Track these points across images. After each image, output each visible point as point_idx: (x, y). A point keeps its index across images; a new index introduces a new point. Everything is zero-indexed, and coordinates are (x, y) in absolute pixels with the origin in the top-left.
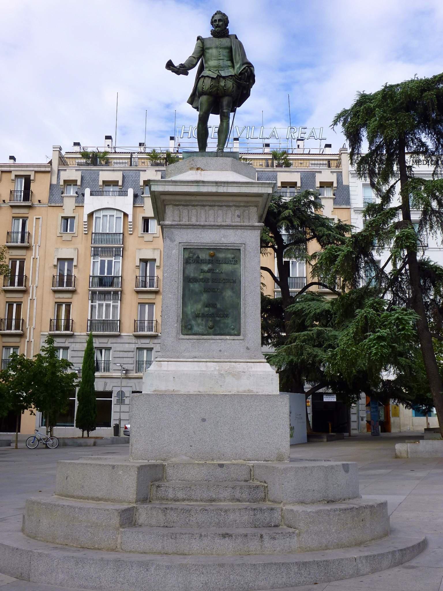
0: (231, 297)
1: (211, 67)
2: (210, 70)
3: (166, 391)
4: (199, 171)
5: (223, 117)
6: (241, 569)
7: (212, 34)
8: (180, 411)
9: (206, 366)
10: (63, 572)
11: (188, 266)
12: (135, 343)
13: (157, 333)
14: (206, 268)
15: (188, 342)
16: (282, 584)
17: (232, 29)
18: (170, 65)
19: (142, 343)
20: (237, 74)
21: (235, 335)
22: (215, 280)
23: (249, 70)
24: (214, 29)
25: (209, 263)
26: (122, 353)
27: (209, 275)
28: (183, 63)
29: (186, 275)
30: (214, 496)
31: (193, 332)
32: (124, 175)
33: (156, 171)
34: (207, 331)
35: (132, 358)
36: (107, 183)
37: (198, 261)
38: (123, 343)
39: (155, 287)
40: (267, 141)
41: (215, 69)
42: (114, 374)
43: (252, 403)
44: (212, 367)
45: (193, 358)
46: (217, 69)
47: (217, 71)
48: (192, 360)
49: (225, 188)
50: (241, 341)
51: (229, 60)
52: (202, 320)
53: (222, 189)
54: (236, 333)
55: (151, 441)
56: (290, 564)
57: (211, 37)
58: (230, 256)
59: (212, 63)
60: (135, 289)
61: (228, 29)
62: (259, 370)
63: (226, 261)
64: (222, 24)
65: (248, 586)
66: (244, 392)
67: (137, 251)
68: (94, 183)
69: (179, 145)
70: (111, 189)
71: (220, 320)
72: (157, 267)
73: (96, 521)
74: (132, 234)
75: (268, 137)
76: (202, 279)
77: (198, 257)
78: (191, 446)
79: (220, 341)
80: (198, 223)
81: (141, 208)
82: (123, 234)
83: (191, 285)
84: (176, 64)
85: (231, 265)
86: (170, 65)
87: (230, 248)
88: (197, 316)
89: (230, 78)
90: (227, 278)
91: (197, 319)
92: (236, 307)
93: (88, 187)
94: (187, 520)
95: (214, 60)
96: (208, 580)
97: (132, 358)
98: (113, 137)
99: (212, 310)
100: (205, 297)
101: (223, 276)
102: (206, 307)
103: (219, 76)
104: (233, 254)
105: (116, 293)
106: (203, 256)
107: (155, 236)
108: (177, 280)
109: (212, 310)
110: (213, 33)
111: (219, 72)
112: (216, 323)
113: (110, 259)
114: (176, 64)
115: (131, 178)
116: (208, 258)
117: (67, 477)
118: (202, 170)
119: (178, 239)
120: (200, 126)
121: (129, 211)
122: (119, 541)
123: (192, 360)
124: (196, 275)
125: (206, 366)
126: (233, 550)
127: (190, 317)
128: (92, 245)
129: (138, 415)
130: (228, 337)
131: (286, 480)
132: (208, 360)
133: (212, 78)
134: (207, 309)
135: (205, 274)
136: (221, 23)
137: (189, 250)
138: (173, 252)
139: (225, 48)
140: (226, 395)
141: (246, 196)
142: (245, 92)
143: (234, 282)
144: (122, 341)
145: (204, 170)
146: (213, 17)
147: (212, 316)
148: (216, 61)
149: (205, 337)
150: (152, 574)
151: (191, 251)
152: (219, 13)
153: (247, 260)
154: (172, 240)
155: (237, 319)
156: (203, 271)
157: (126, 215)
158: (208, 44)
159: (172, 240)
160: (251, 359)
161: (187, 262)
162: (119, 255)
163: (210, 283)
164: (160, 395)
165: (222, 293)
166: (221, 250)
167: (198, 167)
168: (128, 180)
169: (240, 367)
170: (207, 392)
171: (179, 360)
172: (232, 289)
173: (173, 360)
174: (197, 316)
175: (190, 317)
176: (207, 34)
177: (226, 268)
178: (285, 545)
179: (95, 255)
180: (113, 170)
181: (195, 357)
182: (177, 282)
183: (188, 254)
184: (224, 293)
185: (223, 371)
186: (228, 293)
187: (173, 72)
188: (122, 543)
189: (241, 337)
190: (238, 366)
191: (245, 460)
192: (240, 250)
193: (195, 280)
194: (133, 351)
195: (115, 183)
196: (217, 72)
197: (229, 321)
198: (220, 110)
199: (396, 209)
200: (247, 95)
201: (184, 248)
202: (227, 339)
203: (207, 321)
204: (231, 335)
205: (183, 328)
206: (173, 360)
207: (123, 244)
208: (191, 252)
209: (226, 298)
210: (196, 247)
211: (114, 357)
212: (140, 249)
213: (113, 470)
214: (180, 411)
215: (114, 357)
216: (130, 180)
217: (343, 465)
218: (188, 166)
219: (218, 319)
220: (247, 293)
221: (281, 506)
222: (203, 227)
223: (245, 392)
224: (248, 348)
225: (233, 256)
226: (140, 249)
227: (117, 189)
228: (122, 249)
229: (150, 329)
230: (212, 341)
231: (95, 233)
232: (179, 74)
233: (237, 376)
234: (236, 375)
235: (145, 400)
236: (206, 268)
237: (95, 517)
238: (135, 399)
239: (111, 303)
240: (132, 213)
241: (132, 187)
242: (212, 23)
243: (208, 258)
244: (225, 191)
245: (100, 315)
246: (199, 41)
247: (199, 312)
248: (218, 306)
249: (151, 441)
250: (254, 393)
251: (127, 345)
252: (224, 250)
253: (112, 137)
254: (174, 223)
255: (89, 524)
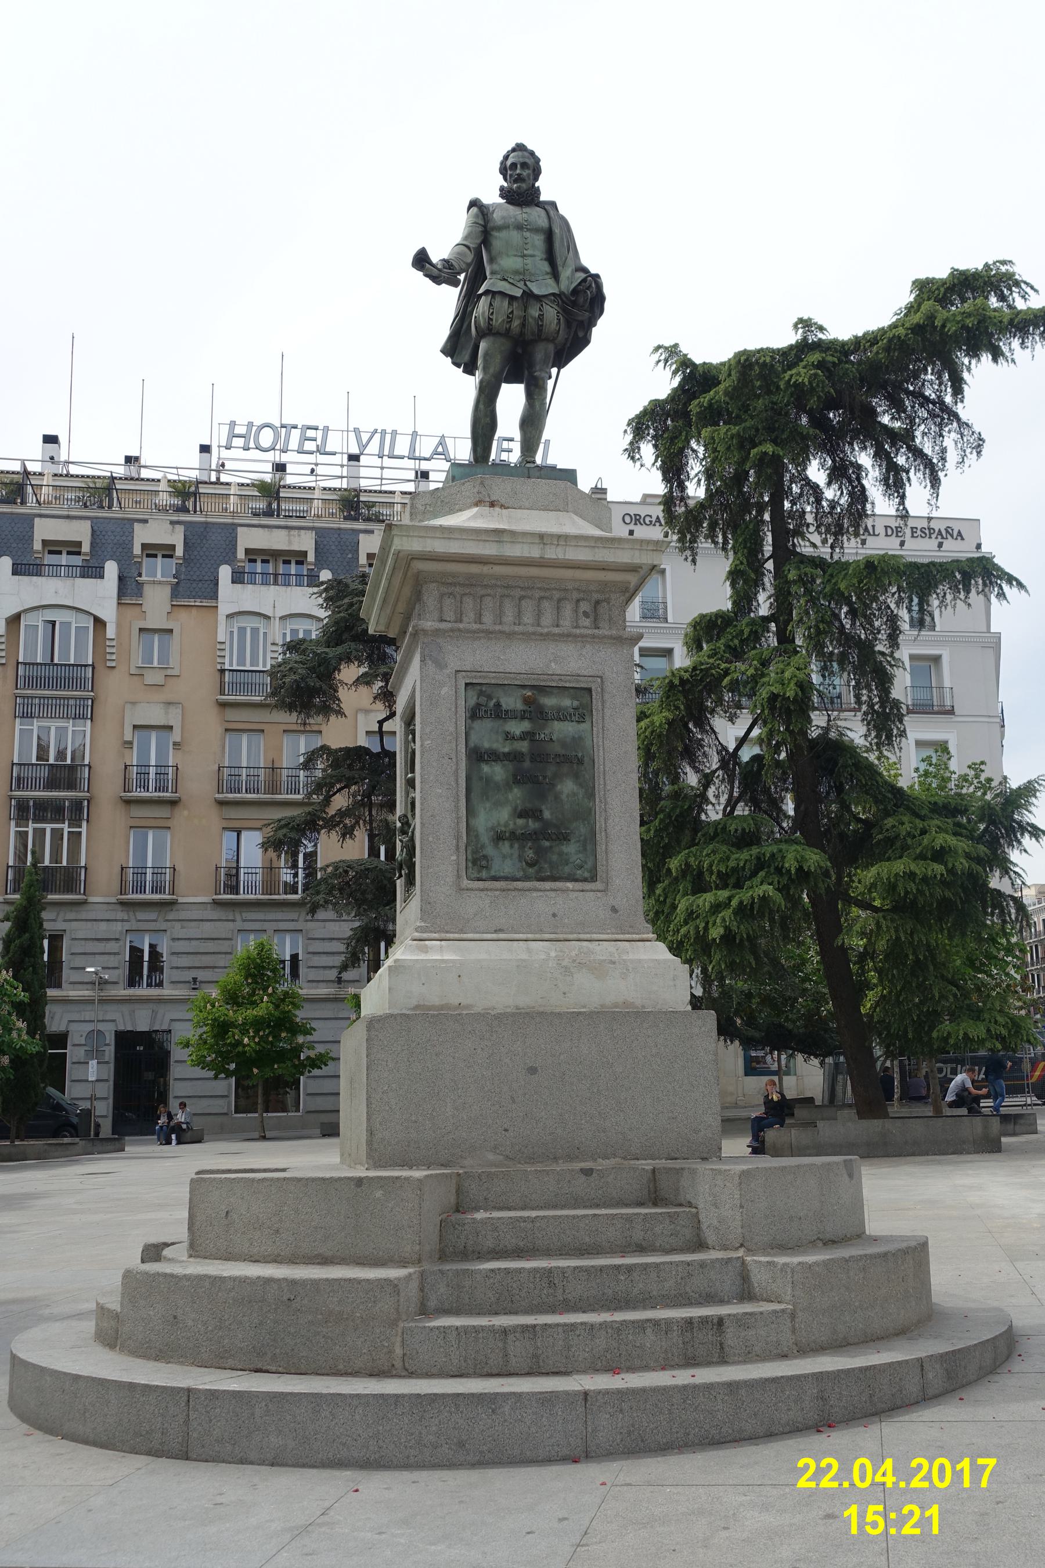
0: (574, 794)
1: (506, 271)
2: (505, 280)
3: (442, 1007)
4: (497, 509)
5: (532, 388)
6: (704, 1395)
7: (502, 196)
8: (479, 1051)
9: (528, 948)
10: (280, 1431)
11: (477, 724)
12: (123, 921)
13: (174, 897)
14: (517, 728)
15: (482, 894)
16: (788, 1424)
17: (547, 188)
18: (421, 260)
19: (139, 921)
20: (566, 292)
21: (585, 880)
22: (539, 757)
23: (593, 285)
24: (505, 185)
25: (523, 718)
26: (91, 943)
27: (524, 746)
28: (446, 257)
29: (472, 745)
30: (587, 1239)
31: (493, 873)
32: (95, 528)
33: (172, 523)
34: (524, 870)
35: (115, 954)
36: (53, 547)
37: (499, 713)
38: (95, 920)
39: (170, 790)
40: (425, 466)
41: (517, 278)
42: (72, 993)
43: (637, 1031)
44: (541, 951)
45: (496, 932)
46: (521, 277)
47: (523, 283)
48: (494, 936)
49: (560, 549)
50: (599, 894)
51: (545, 260)
52: (512, 847)
53: (552, 553)
54: (587, 875)
55: (416, 1122)
56: (803, 1379)
57: (499, 205)
58: (567, 702)
59: (509, 262)
60: (123, 794)
61: (538, 189)
62: (643, 956)
63: (562, 715)
64: (529, 175)
65: (720, 1433)
66: (616, 1007)
67: (128, 706)
68: (20, 545)
69: (223, 465)
70: (64, 559)
71: (551, 847)
72: (175, 744)
73: (337, 1309)
74: (113, 667)
75: (428, 456)
76: (509, 753)
77: (498, 705)
78: (506, 1130)
79: (553, 894)
80: (498, 628)
81: (138, 607)
82: (93, 666)
83: (486, 768)
84: (436, 256)
85: (571, 724)
86: (421, 260)
87: (567, 685)
88: (498, 838)
89: (551, 301)
90: (562, 752)
91: (501, 843)
92: (586, 814)
93: (8, 552)
94: (544, 1296)
95: (515, 256)
96: (633, 1426)
97: (115, 954)
98: (63, 439)
99: (533, 825)
100: (516, 794)
101: (558, 749)
102: (520, 816)
103: (528, 295)
104: (574, 698)
105: (77, 806)
106: (511, 702)
107: (169, 672)
108: (453, 756)
109: (533, 825)
110: (504, 193)
111: (525, 285)
112: (540, 852)
113: (61, 723)
114: (436, 256)
115: (113, 538)
116: (520, 706)
117: (227, 1212)
118: (502, 506)
119: (453, 664)
120: (481, 406)
121: (108, 612)
122: (398, 1351)
123: (494, 936)
124: (495, 746)
125: (528, 948)
126: (663, 1355)
127: (485, 838)
128: (18, 691)
129: (384, 1063)
130: (570, 885)
131: (748, 1198)
132: (530, 936)
133: (512, 298)
134: (521, 822)
135: (515, 742)
136: (525, 173)
137: (479, 688)
138: (443, 692)
139: (537, 230)
140: (580, 1013)
141: (604, 569)
142: (581, 334)
143: (580, 762)
144: (92, 915)
145: (508, 508)
146: (506, 157)
147: (534, 837)
148: (520, 260)
149: (519, 884)
150: (505, 1421)
151: (481, 690)
152: (520, 148)
153: (608, 712)
154: (440, 665)
155: (589, 843)
156: (508, 737)
157: (99, 623)
158: (497, 217)
159: (440, 665)
160: (623, 932)
161: (474, 714)
162: (84, 718)
163: (527, 764)
164: (433, 1016)
165: (553, 785)
166: (548, 689)
167: (493, 498)
168: (103, 541)
169: (603, 951)
170: (533, 1008)
171: (465, 936)
172: (576, 776)
173: (451, 936)
174: (498, 838)
175: (485, 838)
176: (491, 197)
177: (562, 730)
178: (769, 1339)
179: (27, 716)
180: (68, 517)
181: (501, 931)
182: (454, 760)
183: (475, 698)
184: (559, 787)
185: (567, 960)
186: (567, 787)
187: (426, 275)
188: (404, 1355)
189: (598, 885)
190: (598, 948)
191: (625, 1158)
192: (589, 690)
193: (493, 756)
194: (117, 939)
195: (74, 548)
196: (521, 284)
197: (571, 849)
198: (526, 373)
199: (766, 620)
200: (585, 341)
201: (467, 684)
202: (568, 890)
203: (522, 848)
204: (576, 880)
205: (470, 865)
206: (451, 936)
207: (92, 691)
208: (481, 693)
209: (564, 797)
210: (493, 682)
211: (72, 954)
212: (134, 703)
213: (359, 1190)
214: (479, 1051)
215: (72, 954)
216: (109, 541)
217: (845, 1161)
218: (469, 497)
219: (547, 844)
220: (608, 788)
221: (740, 1255)
222: (510, 635)
223: (616, 1005)
224: (614, 910)
225: (576, 703)
226: (134, 703)
227: (77, 560)
228: (90, 701)
229: (157, 889)
230: (535, 894)
231: (25, 664)
232: (439, 283)
233: (599, 969)
234: (596, 969)
235: (399, 1027)
236: (517, 728)
237: (336, 1299)
238: (376, 1025)
239: (66, 828)
240: (114, 620)
241: (115, 557)
242: (503, 171)
243: (520, 706)
244: (561, 556)
245: (56, 856)
246: (474, 210)
247: (503, 829)
248: (547, 815)
249: (416, 1122)
250: (637, 1008)
251: (103, 926)
252: (555, 691)
253: (61, 439)
254: (444, 626)
255: (320, 1317)
